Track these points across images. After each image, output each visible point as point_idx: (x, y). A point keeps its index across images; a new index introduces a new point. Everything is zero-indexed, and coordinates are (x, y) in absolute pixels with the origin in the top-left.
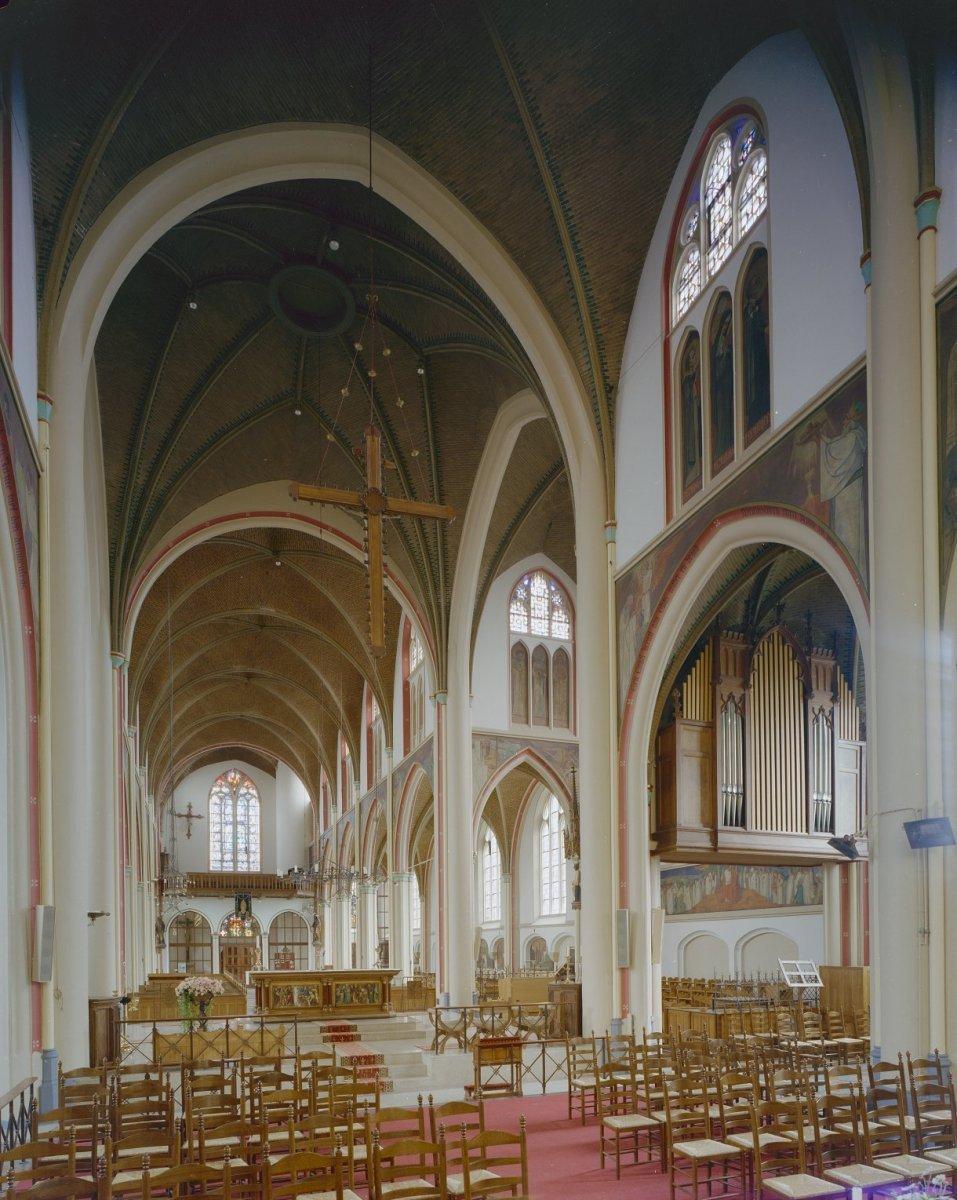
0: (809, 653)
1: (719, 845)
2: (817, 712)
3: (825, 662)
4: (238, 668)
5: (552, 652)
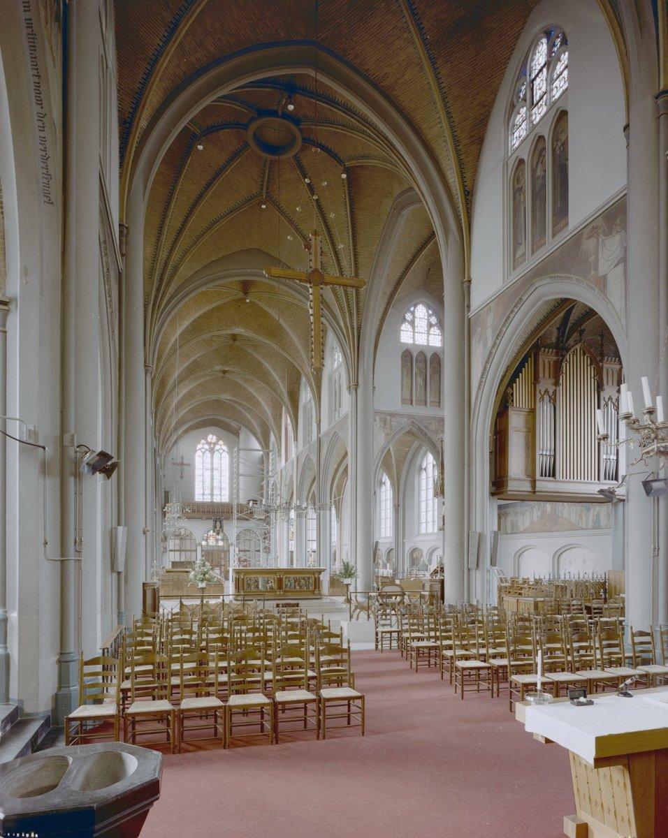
0: (602, 361)
1: (537, 489)
2: (607, 400)
3: (612, 366)
4: (218, 368)
5: (429, 356)
